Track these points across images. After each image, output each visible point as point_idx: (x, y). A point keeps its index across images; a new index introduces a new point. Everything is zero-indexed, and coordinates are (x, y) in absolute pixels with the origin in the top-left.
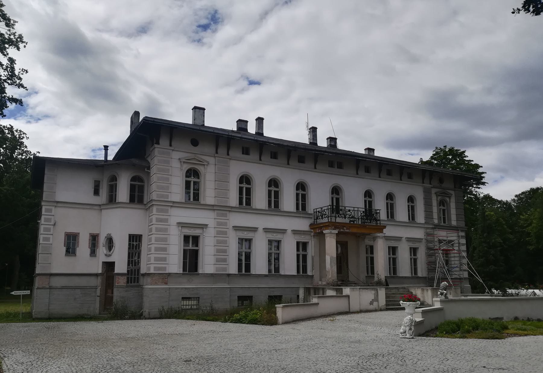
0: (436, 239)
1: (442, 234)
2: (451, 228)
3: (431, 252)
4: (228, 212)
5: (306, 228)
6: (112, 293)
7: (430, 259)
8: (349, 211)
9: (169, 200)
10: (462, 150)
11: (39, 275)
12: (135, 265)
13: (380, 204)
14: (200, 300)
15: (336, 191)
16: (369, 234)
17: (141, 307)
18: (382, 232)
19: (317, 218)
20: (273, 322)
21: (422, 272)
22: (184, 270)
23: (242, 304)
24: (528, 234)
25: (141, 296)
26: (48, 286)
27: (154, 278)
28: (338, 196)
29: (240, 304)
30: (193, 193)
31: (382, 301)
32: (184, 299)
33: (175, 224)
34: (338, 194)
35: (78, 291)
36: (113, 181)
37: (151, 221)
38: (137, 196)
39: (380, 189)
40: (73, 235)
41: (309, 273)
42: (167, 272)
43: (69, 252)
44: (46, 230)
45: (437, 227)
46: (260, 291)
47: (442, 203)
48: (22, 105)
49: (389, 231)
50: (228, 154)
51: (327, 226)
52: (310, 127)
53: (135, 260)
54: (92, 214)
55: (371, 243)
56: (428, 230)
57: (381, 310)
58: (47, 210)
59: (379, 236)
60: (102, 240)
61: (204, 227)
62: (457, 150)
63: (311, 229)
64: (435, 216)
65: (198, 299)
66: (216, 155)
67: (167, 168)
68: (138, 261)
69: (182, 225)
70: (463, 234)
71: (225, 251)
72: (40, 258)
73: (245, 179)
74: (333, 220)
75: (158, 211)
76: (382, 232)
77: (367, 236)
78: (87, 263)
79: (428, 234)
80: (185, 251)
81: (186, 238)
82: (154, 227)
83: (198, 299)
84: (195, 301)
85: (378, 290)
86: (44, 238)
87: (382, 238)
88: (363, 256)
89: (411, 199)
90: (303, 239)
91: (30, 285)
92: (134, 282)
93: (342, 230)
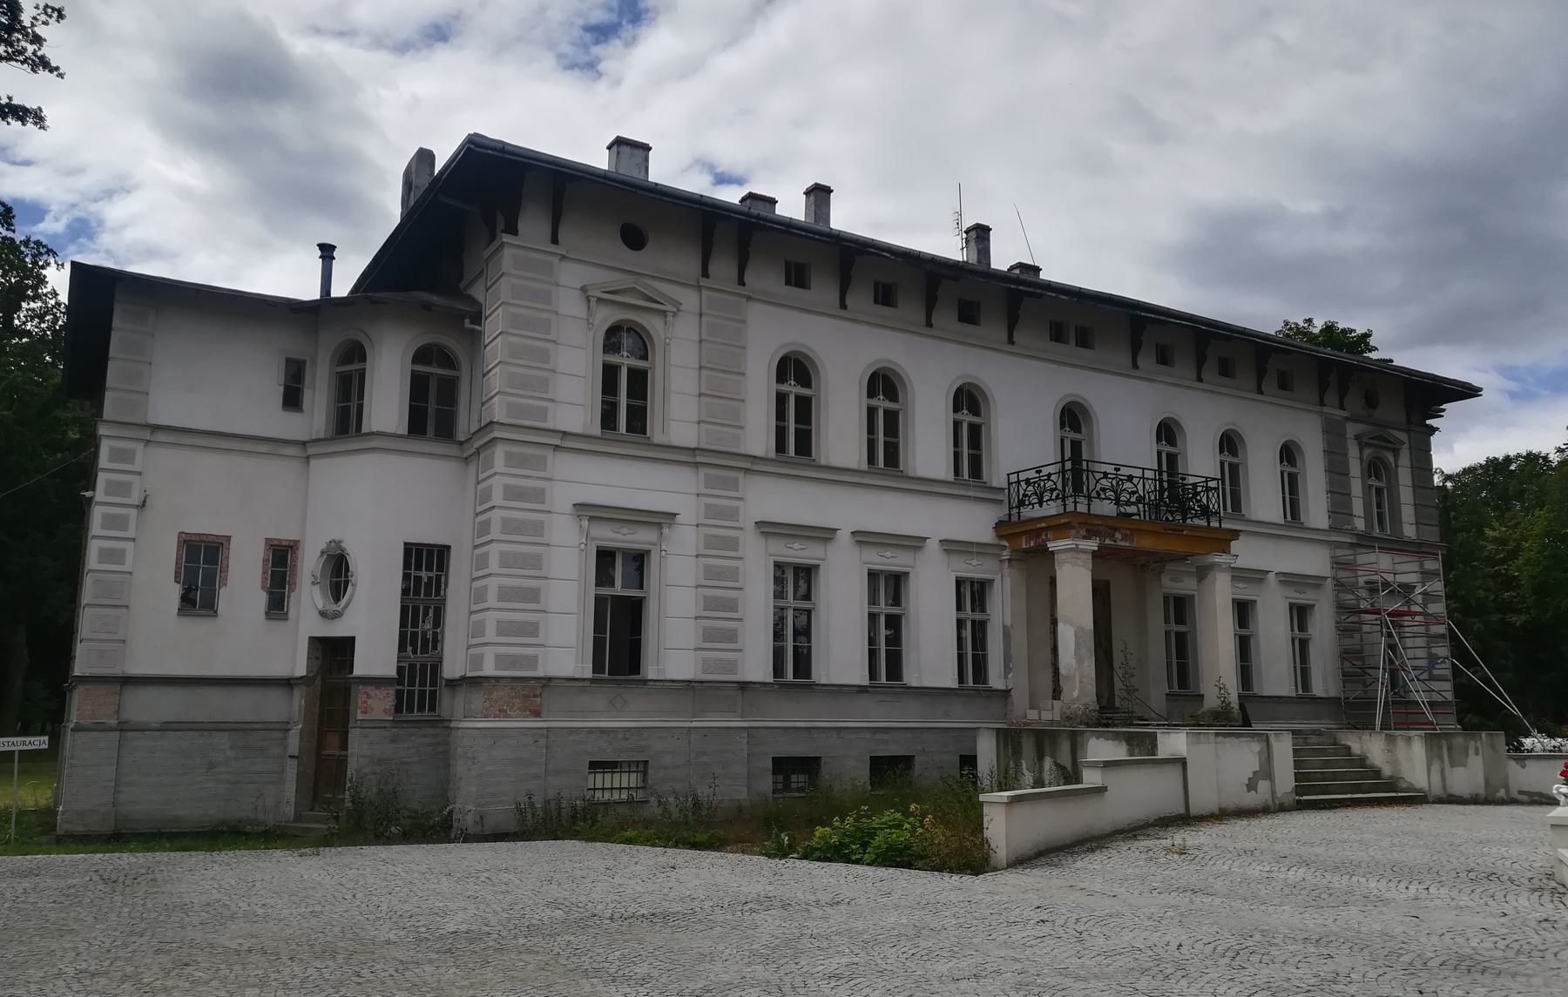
0: (1361, 580)
1: (1382, 563)
2: (1397, 546)
3: (1353, 619)
4: (741, 475)
5: (986, 535)
6: (344, 745)
7: (1347, 641)
8: (1130, 478)
9: (550, 425)
10: (1360, 330)
11: (83, 680)
12: (425, 649)
13: (1201, 462)
14: (650, 771)
15: (1073, 417)
16: (1183, 558)
17: (443, 793)
18: (1226, 550)
19: (1021, 503)
20: (970, 858)
21: (1324, 683)
22: (598, 666)
23: (787, 787)
24: (1510, 582)
25: (443, 757)
26: (113, 722)
27: (494, 696)
28: (1076, 436)
29: (780, 786)
30: (626, 405)
31: (1285, 779)
32: (595, 766)
33: (569, 508)
34: (1078, 430)
35: (222, 740)
36: (350, 362)
37: (486, 495)
38: (434, 413)
39: (1204, 417)
40: (201, 551)
41: (996, 680)
42: (540, 673)
43: (193, 603)
44: (110, 522)
45: (1364, 542)
46: (847, 739)
47: (1374, 468)
48: (42, 128)
49: (1246, 553)
50: (741, 282)
51: (1059, 526)
52: (968, 223)
53: (424, 634)
54: (278, 474)
55: (1186, 586)
56: (1339, 552)
57: (1282, 809)
58: (119, 456)
59: (1219, 564)
60: (310, 563)
61: (661, 520)
62: (1344, 331)
63: (1000, 537)
64: (1358, 507)
65: (643, 767)
66: (704, 282)
67: (544, 316)
68: (435, 635)
69: (589, 512)
70: (1433, 565)
71: (731, 605)
72: (88, 623)
73: (795, 369)
74: (1082, 508)
75: (510, 459)
76: (1226, 550)
77: (1169, 567)
78: (253, 641)
79: (1337, 564)
80: (600, 601)
81: (605, 558)
82: (496, 517)
83: (643, 767)
84: (633, 776)
85: (1272, 739)
86: (105, 516)
87: (1225, 570)
88: (1157, 625)
89: (1289, 454)
90: (976, 569)
91: (51, 719)
92: (421, 708)
93: (1108, 541)
